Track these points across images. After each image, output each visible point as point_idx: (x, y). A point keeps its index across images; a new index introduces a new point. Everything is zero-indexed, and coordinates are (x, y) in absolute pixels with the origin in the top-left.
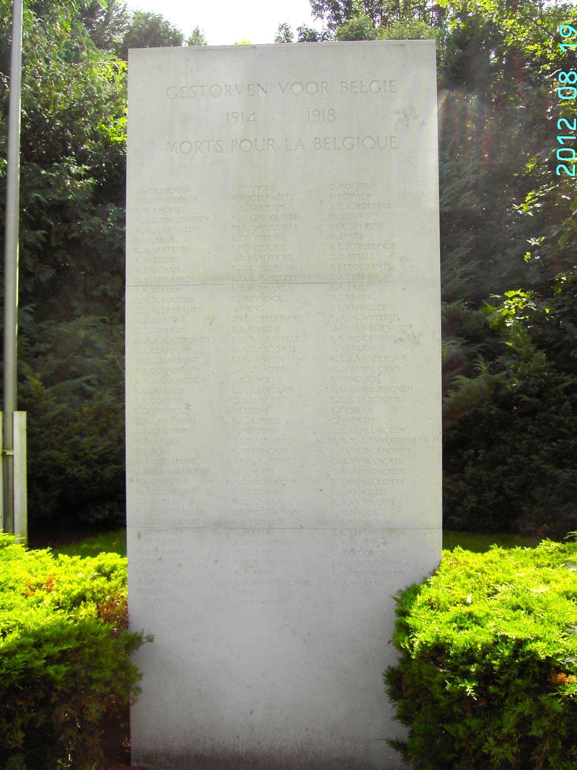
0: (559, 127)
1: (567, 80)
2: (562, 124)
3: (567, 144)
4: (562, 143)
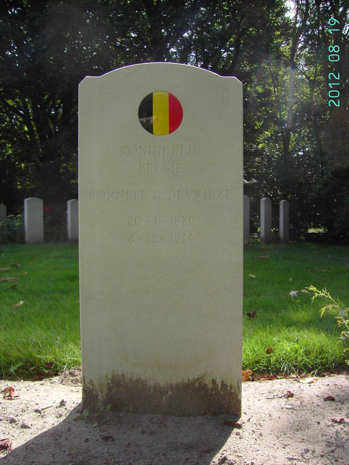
0: (330, 105)
1: (334, 49)
2: (332, 76)
3: (335, 87)
4: (331, 87)
